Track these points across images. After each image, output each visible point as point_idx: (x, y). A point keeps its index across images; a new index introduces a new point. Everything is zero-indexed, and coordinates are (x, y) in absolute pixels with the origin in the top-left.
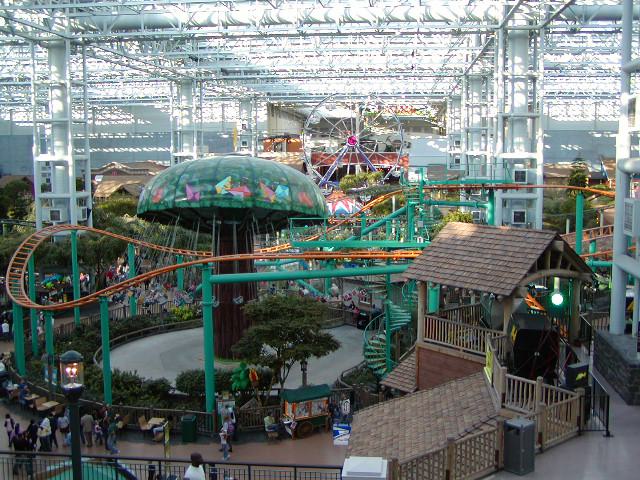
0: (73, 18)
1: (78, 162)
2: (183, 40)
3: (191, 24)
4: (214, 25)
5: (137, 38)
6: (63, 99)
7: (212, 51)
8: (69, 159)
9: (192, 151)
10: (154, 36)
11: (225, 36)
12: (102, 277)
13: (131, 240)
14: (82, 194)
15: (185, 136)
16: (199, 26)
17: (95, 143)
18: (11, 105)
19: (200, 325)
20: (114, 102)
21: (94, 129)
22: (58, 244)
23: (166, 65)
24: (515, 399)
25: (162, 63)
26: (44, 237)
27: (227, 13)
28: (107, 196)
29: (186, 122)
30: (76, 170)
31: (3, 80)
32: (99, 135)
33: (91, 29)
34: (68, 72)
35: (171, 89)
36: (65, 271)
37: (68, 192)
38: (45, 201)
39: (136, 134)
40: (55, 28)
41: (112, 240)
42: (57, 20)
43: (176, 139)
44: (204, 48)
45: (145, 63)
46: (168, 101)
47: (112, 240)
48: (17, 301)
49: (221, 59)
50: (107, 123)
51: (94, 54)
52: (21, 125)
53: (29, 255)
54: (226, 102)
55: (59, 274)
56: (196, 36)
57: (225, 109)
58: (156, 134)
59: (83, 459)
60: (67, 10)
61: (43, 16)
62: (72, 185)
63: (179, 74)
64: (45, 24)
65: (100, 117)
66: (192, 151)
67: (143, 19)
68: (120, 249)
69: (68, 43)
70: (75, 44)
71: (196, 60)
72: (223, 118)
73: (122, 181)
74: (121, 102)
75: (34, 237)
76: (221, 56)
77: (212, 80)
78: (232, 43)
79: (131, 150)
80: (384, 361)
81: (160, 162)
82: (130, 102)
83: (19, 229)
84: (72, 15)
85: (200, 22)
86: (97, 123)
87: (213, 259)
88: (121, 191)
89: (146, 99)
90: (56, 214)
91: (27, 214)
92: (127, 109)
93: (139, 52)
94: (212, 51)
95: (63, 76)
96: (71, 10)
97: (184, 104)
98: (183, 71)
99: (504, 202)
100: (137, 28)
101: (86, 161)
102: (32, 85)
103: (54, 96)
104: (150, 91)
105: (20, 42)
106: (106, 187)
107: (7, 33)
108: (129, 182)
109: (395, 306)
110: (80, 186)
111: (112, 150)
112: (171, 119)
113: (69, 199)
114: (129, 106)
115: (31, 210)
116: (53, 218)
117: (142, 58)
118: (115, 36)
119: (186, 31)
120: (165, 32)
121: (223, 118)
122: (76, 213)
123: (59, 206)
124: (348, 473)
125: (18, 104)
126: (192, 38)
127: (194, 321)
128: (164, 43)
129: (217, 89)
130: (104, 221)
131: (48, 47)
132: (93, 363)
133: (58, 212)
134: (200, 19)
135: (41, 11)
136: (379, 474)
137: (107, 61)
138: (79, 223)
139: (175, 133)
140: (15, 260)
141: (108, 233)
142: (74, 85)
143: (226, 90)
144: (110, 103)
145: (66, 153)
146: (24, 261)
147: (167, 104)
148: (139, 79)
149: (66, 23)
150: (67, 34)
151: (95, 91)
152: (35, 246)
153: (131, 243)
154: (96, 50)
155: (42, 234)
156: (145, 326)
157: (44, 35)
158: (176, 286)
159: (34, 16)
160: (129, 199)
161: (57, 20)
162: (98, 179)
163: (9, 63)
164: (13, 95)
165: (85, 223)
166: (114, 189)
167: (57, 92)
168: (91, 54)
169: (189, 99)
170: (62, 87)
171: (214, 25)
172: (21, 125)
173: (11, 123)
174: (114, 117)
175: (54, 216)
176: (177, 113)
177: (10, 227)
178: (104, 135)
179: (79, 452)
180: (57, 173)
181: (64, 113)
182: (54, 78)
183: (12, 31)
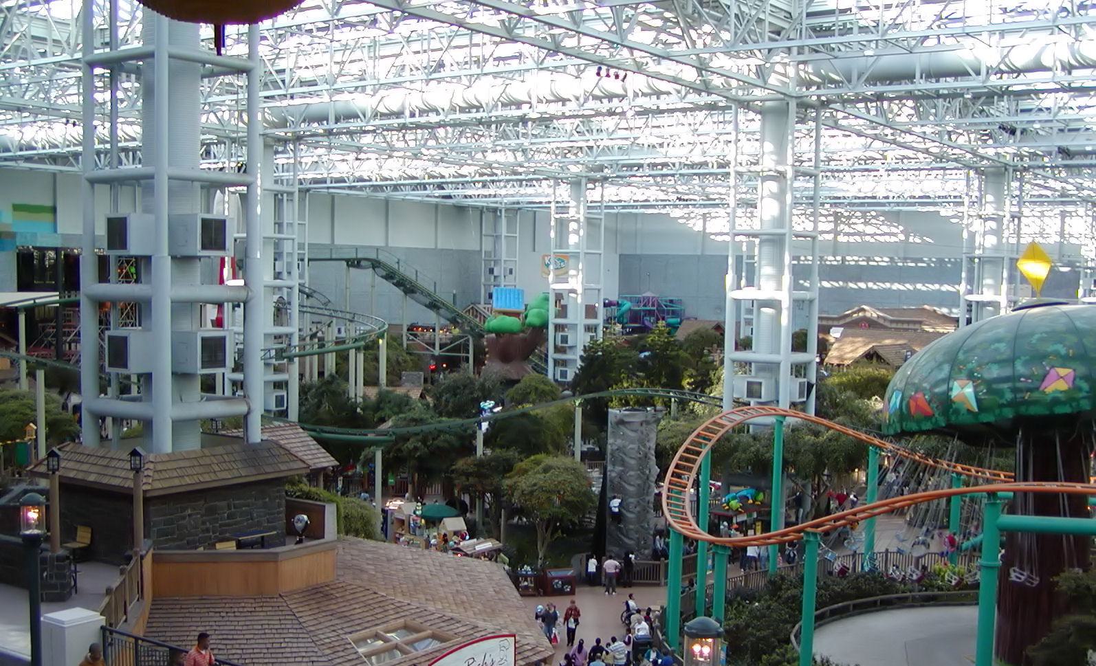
0: (805, 62)
1: (799, 305)
2: (991, 96)
3: (1003, 67)
4: (1049, 69)
5: (910, 95)
6: (780, 197)
7: (1044, 116)
8: (784, 297)
9: (998, 293)
10: (937, 91)
11: (1068, 89)
12: (824, 500)
13: (877, 441)
14: (800, 357)
15: (987, 267)
16: (1019, 72)
17: (829, 272)
18: (705, 206)
19: (974, 601)
20: (870, 204)
21: (835, 248)
22: (755, 438)
23: (962, 140)
25: (954, 137)
26: (730, 425)
27: (1071, 47)
28: (846, 363)
29: (991, 241)
30: (794, 317)
32: (844, 260)
33: (832, 81)
34: (790, 152)
35: (968, 185)
36: (763, 483)
37: (779, 353)
38: (745, 365)
39: (905, 259)
40: (773, 80)
41: (843, 438)
42: (779, 68)
43: (971, 271)
44: (1030, 110)
45: (924, 136)
46: (962, 204)
47: (843, 438)
48: (677, 526)
49: (1061, 130)
50: (858, 239)
51: (836, 122)
52: (719, 238)
54: (1070, 208)
55: (752, 487)
56: (1015, 88)
57: (1067, 220)
58: (941, 261)
60: (795, 51)
61: (754, 62)
62: (786, 341)
63: (983, 158)
64: (757, 73)
65: (847, 229)
66: (998, 293)
67: (919, 61)
68: (856, 456)
69: (793, 105)
70: (804, 105)
71: (1013, 132)
72: (1062, 234)
73: (877, 339)
74: (883, 205)
75: (714, 423)
76: (1062, 126)
77: (1044, 167)
78: (1083, 101)
79: (896, 286)
81: (945, 311)
82: (898, 204)
83: (698, 408)
84: (802, 58)
85: (1019, 64)
86: (842, 239)
87: (1006, 487)
88: (871, 356)
89: (925, 200)
90: (756, 387)
91: (712, 384)
92: (894, 217)
93: (915, 119)
94: (1044, 116)
95: (781, 160)
96: (801, 50)
97: (989, 210)
98: (991, 152)
100: (910, 77)
101: (811, 301)
102: (733, 174)
103: (766, 193)
104: (932, 185)
105: (720, 104)
106: (848, 348)
107: (698, 91)
108: (888, 342)
110: (799, 343)
111: (862, 285)
112: (965, 235)
113: (778, 364)
114: (895, 212)
115: (719, 379)
116: (750, 393)
117: (917, 129)
118: (870, 91)
119: (994, 80)
120: (961, 83)
121: (1062, 234)
122: (789, 389)
123: (762, 374)
125: (717, 205)
126: (1004, 93)
127: (964, 593)
128: (957, 103)
129: (1051, 183)
130: (835, 405)
131: (759, 112)
132: (788, 641)
133: (760, 383)
134: (1020, 58)
135: (751, 53)
137: (859, 134)
138: (793, 405)
139: (971, 260)
140: (681, 458)
141: (838, 427)
142: (798, 174)
143: (1069, 187)
144: (866, 204)
145: (779, 287)
146: (694, 461)
147: (960, 209)
148: (913, 165)
149: (791, 71)
150: (794, 90)
151: (841, 185)
152: (716, 437)
153: (877, 447)
154: (840, 115)
155: (729, 417)
156: (886, 590)
157: (758, 93)
158: (947, 527)
159: (740, 62)
160: (883, 371)
161: (779, 68)
162: (836, 333)
163: (702, 139)
164: (708, 190)
165: (803, 406)
166: (861, 351)
167: (773, 186)
168: (831, 123)
169: (999, 202)
170: (780, 177)
171: (1049, 69)
172: (719, 238)
173: (704, 234)
174: (870, 229)
175: (753, 390)
176: (977, 226)
177: (683, 403)
178: (851, 260)
180: (763, 318)
181: (780, 220)
182: (769, 163)
183: (707, 88)
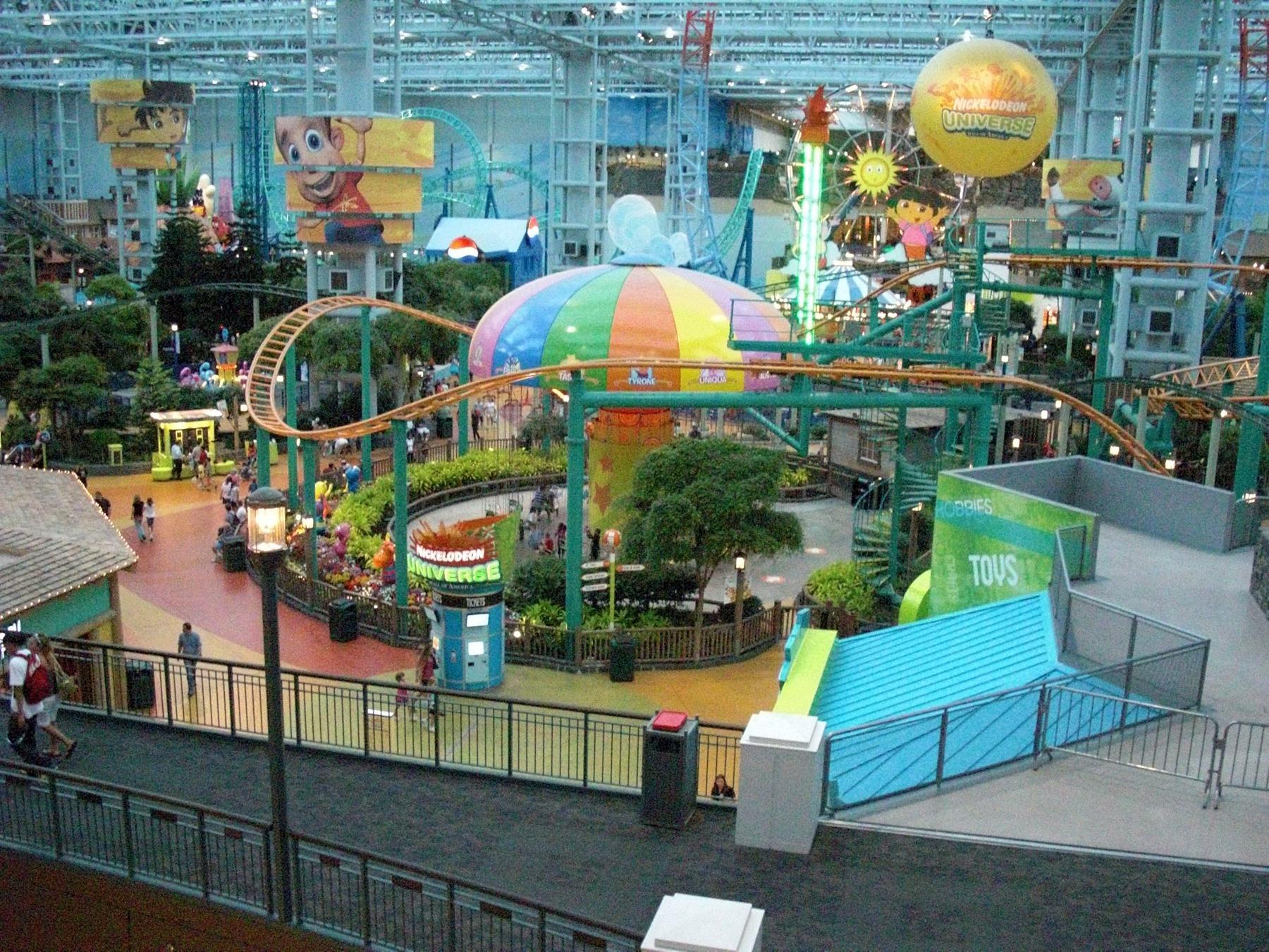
24: (1040, 651)
31: (452, 948)
53: (288, 345)
59: (283, 676)
80: (885, 564)
99: (1135, 294)
109: (912, 467)
124: (752, 738)
136: (807, 745)
152: (298, 331)
179: (278, 665)
